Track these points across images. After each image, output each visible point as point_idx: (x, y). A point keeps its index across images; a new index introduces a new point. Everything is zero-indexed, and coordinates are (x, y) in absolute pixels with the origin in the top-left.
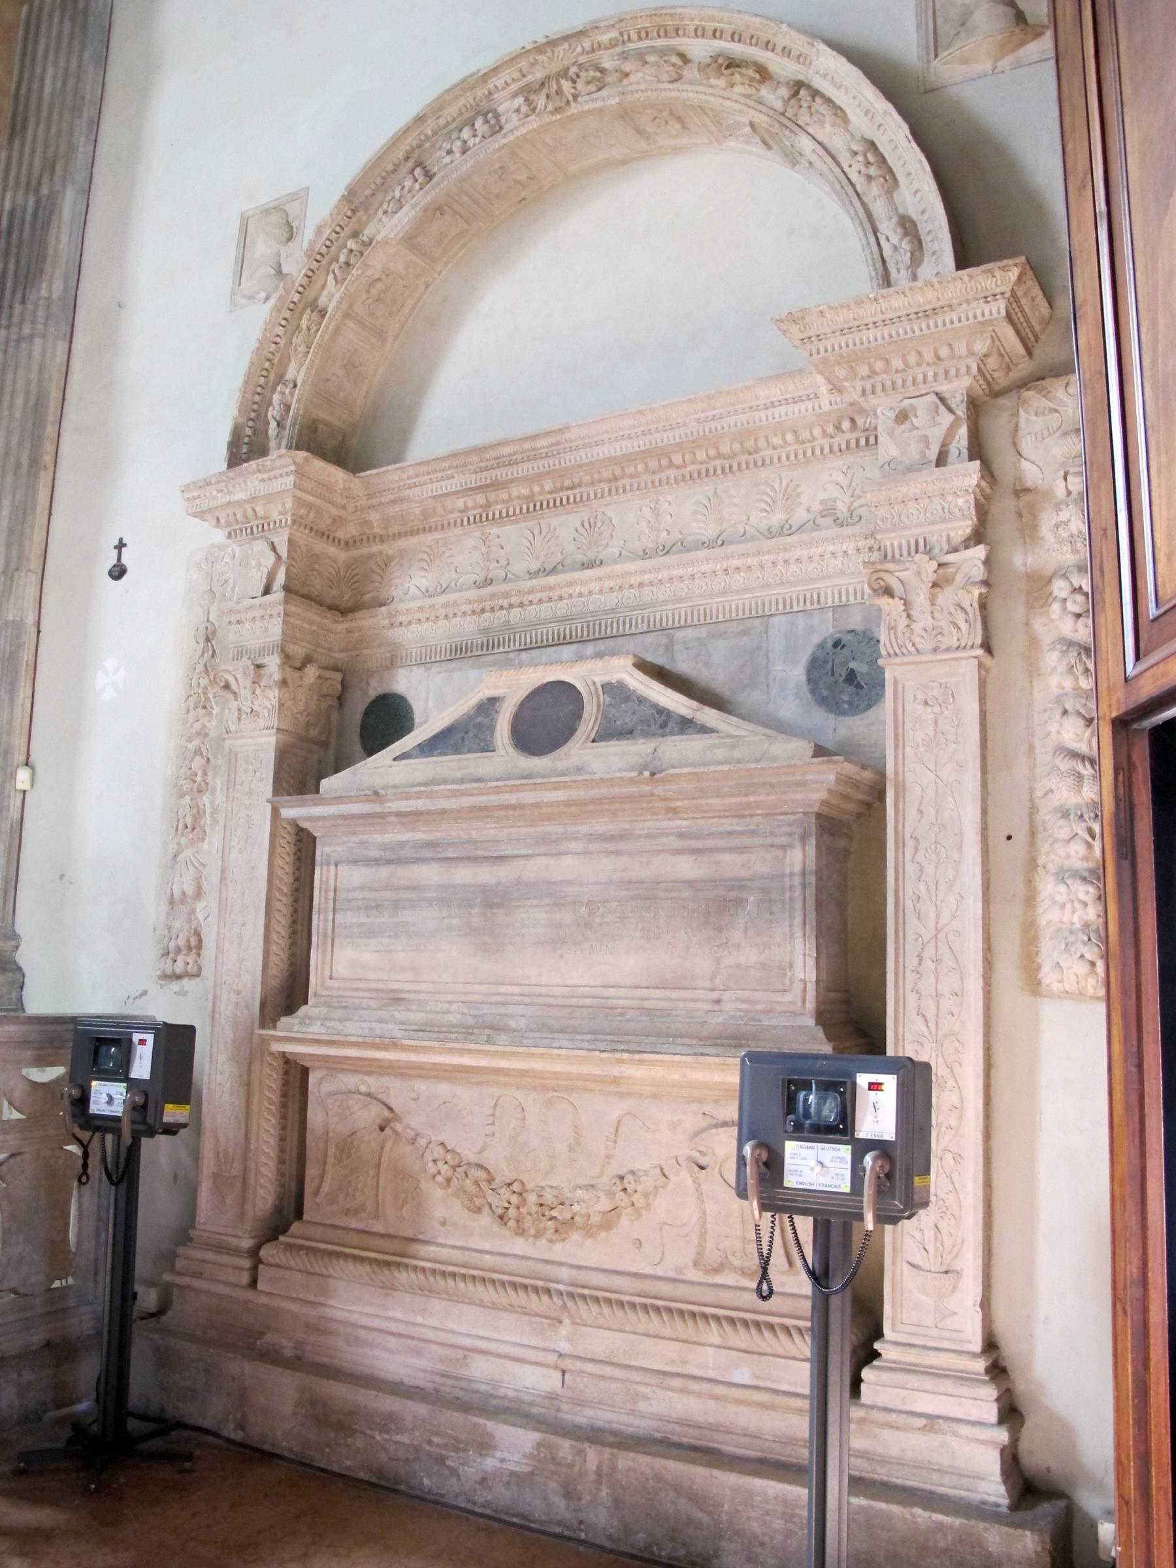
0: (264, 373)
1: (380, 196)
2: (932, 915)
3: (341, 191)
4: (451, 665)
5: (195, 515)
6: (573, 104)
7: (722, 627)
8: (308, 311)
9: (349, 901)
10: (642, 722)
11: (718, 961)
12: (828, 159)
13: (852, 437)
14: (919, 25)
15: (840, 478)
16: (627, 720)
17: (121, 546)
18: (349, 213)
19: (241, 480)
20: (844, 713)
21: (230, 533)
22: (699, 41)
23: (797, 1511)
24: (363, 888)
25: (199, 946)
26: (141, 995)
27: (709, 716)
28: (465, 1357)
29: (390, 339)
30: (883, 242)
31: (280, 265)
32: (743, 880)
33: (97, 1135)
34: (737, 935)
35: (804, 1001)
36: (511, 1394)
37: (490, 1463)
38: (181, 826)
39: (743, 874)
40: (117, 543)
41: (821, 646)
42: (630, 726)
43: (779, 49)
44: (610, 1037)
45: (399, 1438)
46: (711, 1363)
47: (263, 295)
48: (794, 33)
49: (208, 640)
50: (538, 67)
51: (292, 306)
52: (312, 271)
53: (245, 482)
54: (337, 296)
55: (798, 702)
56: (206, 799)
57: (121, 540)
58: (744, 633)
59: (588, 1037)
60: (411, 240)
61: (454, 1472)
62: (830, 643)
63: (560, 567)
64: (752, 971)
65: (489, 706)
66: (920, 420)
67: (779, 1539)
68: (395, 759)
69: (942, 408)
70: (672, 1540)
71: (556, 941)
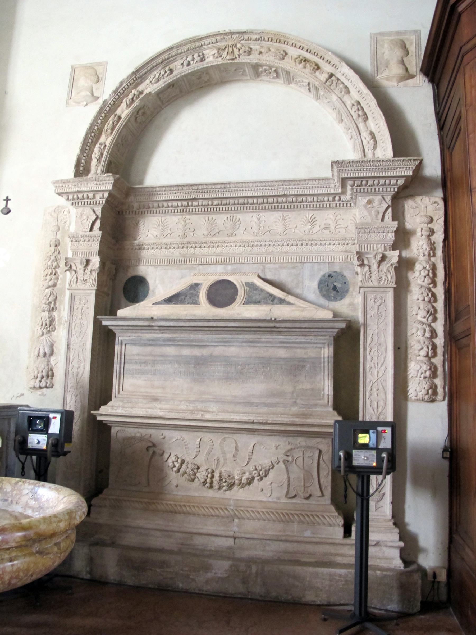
2: (376, 374)
4: (167, 267)
5: (57, 194)
6: (238, 58)
7: (285, 265)
9: (131, 359)
10: (264, 299)
11: (295, 387)
12: (343, 105)
13: (338, 203)
14: (371, 63)
15: (332, 217)
16: (257, 297)
17: (7, 200)
19: (85, 183)
20: (332, 301)
21: (72, 203)
22: (293, 48)
23: (335, 577)
24: (138, 355)
25: (53, 376)
26: (20, 396)
27: (290, 299)
28: (192, 537)
30: (363, 139)
32: (304, 359)
33: (29, 457)
34: (302, 378)
35: (328, 402)
36: (213, 549)
37: (209, 575)
38: (44, 325)
39: (305, 356)
40: (5, 198)
41: (324, 276)
42: (259, 300)
43: (326, 60)
44: (254, 415)
45: (168, 570)
46: (295, 530)
47: (85, 103)
48: (333, 56)
49: (56, 246)
50: (224, 40)
53: (87, 184)
55: (314, 295)
56: (55, 314)
57: (7, 197)
58: (294, 268)
59: (245, 415)
61: (193, 580)
62: (327, 275)
63: (217, 234)
64: (308, 391)
65: (195, 287)
66: (376, 203)
67: (327, 588)
68: (153, 304)
69: (383, 201)
70: (286, 593)
71: (227, 379)
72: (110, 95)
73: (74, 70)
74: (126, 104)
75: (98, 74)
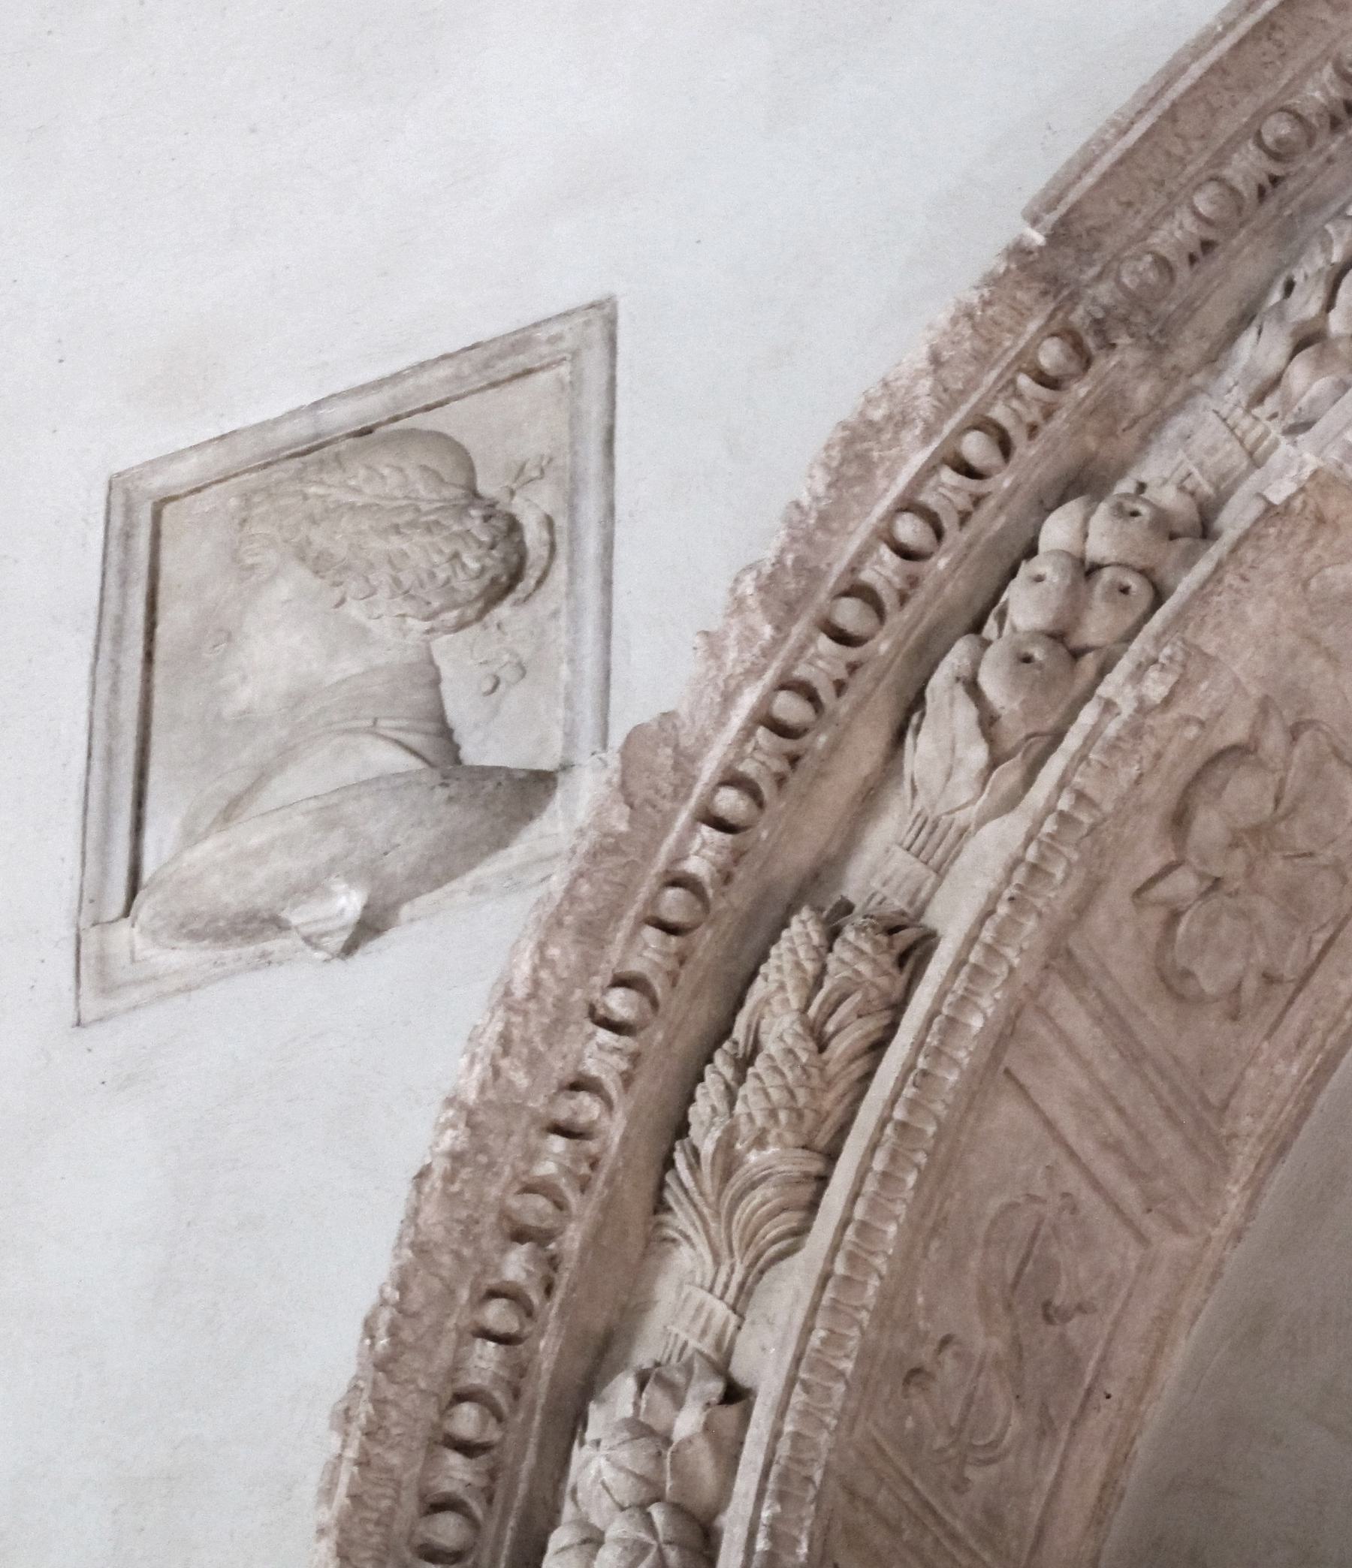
0: (497, 1315)
1: (1245, 264)
3: (1007, 223)
8: (803, 929)
18: (1051, 355)
29: (1244, 1157)
31: (445, 732)
47: (348, 903)
51: (674, 904)
52: (807, 692)
54: (996, 842)
60: (516, 966)
72: (713, 644)
73: (141, 527)
74: (966, 714)
75: (487, 486)
